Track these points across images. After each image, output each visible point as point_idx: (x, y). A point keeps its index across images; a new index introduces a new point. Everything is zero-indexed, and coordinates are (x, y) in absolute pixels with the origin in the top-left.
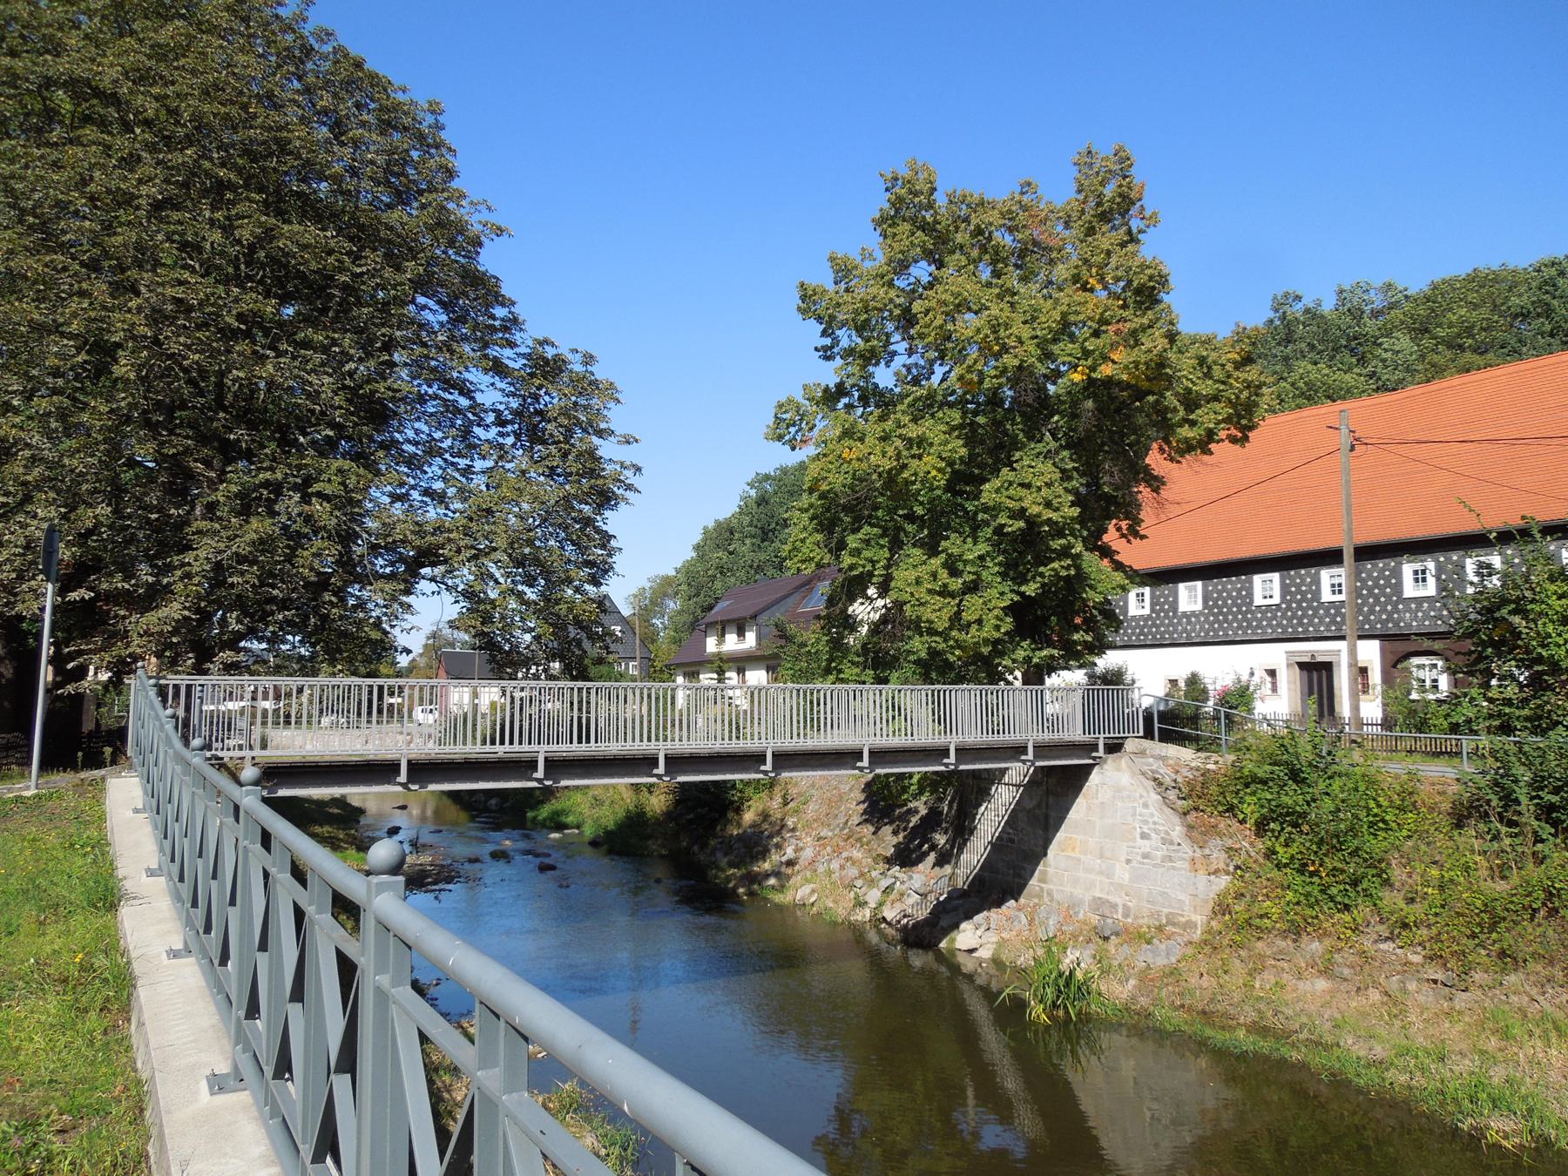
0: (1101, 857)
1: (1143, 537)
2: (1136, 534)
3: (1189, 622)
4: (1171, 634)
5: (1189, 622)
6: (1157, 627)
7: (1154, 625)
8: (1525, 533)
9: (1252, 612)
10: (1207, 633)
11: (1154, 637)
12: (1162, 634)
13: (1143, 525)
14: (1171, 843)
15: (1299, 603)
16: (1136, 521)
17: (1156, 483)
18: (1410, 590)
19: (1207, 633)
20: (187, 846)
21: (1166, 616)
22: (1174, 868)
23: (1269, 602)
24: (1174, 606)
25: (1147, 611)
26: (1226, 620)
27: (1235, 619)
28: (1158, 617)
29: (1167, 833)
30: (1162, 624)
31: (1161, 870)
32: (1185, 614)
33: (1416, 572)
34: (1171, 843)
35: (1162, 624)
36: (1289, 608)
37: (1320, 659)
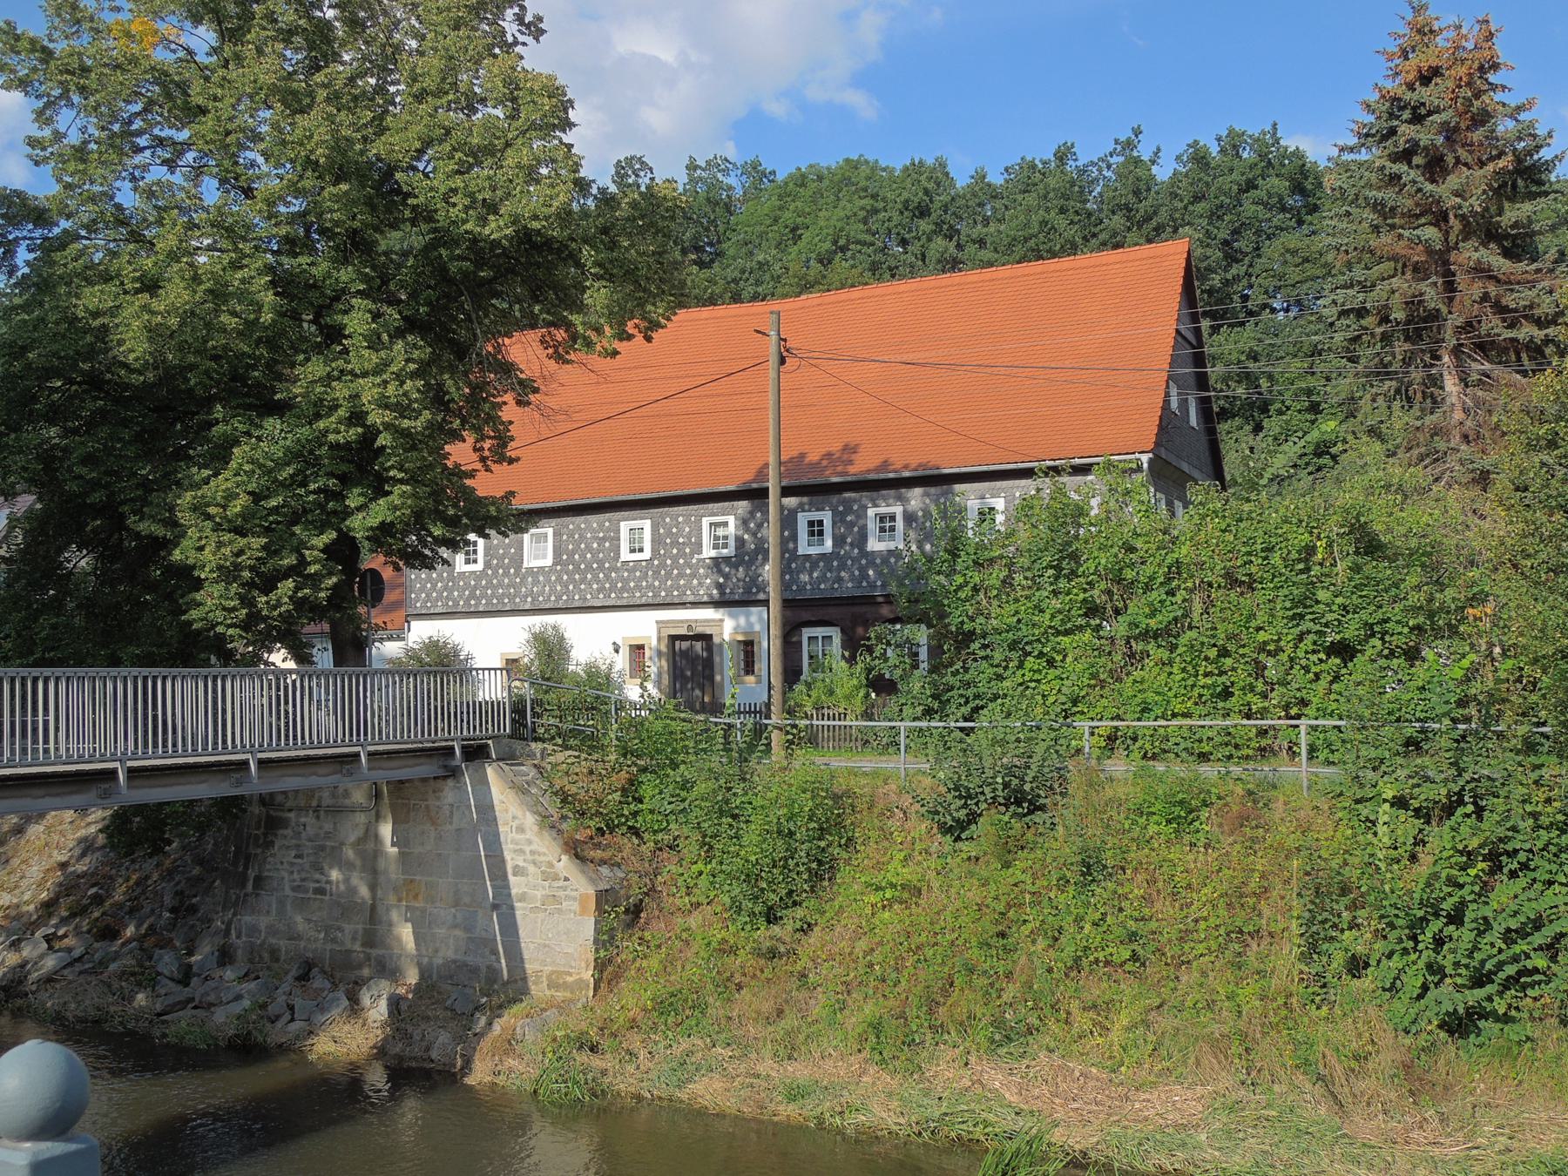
0: (456, 904)
1: (511, 461)
2: (502, 458)
3: (536, 582)
4: (512, 598)
5: (536, 582)
6: (495, 588)
7: (490, 585)
8: (1056, 470)
9: (616, 570)
10: (559, 598)
11: (456, 604)
12: (500, 598)
13: (512, 445)
14: (556, 878)
15: (675, 559)
16: (503, 440)
17: (525, 390)
18: (530, 562)
19: (559, 598)
20: (1013, 1164)
21: (506, 574)
22: (560, 911)
23: (637, 556)
24: (518, 560)
25: (479, 566)
26: (583, 580)
27: (596, 577)
28: (495, 573)
29: (551, 865)
30: (500, 585)
31: (541, 915)
32: (530, 570)
33: (811, 524)
34: (556, 878)
35: (500, 585)
36: (663, 565)
37: (700, 630)
